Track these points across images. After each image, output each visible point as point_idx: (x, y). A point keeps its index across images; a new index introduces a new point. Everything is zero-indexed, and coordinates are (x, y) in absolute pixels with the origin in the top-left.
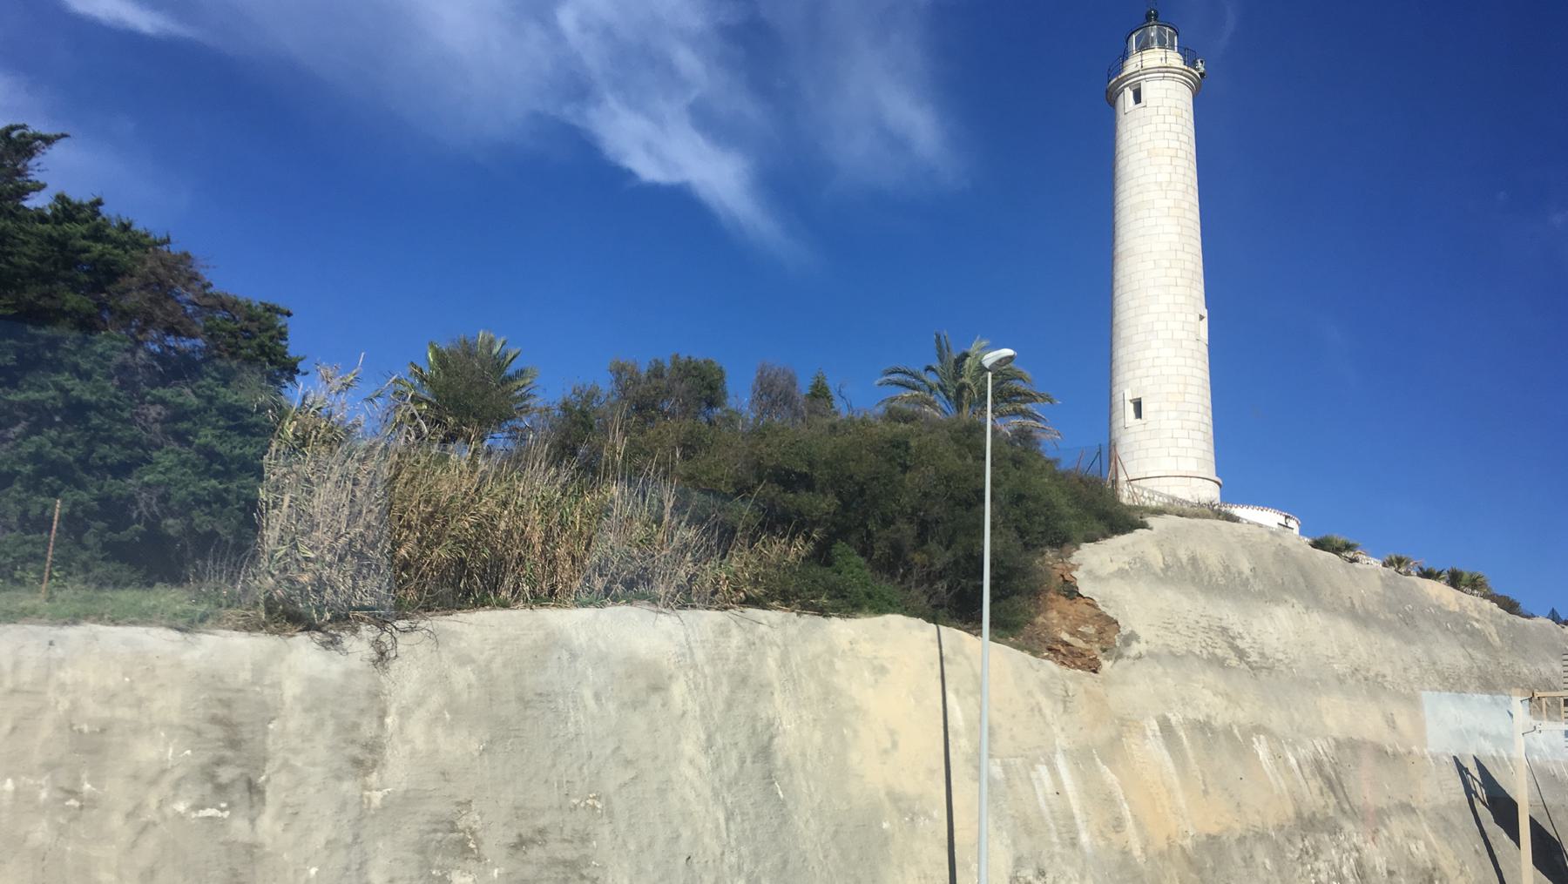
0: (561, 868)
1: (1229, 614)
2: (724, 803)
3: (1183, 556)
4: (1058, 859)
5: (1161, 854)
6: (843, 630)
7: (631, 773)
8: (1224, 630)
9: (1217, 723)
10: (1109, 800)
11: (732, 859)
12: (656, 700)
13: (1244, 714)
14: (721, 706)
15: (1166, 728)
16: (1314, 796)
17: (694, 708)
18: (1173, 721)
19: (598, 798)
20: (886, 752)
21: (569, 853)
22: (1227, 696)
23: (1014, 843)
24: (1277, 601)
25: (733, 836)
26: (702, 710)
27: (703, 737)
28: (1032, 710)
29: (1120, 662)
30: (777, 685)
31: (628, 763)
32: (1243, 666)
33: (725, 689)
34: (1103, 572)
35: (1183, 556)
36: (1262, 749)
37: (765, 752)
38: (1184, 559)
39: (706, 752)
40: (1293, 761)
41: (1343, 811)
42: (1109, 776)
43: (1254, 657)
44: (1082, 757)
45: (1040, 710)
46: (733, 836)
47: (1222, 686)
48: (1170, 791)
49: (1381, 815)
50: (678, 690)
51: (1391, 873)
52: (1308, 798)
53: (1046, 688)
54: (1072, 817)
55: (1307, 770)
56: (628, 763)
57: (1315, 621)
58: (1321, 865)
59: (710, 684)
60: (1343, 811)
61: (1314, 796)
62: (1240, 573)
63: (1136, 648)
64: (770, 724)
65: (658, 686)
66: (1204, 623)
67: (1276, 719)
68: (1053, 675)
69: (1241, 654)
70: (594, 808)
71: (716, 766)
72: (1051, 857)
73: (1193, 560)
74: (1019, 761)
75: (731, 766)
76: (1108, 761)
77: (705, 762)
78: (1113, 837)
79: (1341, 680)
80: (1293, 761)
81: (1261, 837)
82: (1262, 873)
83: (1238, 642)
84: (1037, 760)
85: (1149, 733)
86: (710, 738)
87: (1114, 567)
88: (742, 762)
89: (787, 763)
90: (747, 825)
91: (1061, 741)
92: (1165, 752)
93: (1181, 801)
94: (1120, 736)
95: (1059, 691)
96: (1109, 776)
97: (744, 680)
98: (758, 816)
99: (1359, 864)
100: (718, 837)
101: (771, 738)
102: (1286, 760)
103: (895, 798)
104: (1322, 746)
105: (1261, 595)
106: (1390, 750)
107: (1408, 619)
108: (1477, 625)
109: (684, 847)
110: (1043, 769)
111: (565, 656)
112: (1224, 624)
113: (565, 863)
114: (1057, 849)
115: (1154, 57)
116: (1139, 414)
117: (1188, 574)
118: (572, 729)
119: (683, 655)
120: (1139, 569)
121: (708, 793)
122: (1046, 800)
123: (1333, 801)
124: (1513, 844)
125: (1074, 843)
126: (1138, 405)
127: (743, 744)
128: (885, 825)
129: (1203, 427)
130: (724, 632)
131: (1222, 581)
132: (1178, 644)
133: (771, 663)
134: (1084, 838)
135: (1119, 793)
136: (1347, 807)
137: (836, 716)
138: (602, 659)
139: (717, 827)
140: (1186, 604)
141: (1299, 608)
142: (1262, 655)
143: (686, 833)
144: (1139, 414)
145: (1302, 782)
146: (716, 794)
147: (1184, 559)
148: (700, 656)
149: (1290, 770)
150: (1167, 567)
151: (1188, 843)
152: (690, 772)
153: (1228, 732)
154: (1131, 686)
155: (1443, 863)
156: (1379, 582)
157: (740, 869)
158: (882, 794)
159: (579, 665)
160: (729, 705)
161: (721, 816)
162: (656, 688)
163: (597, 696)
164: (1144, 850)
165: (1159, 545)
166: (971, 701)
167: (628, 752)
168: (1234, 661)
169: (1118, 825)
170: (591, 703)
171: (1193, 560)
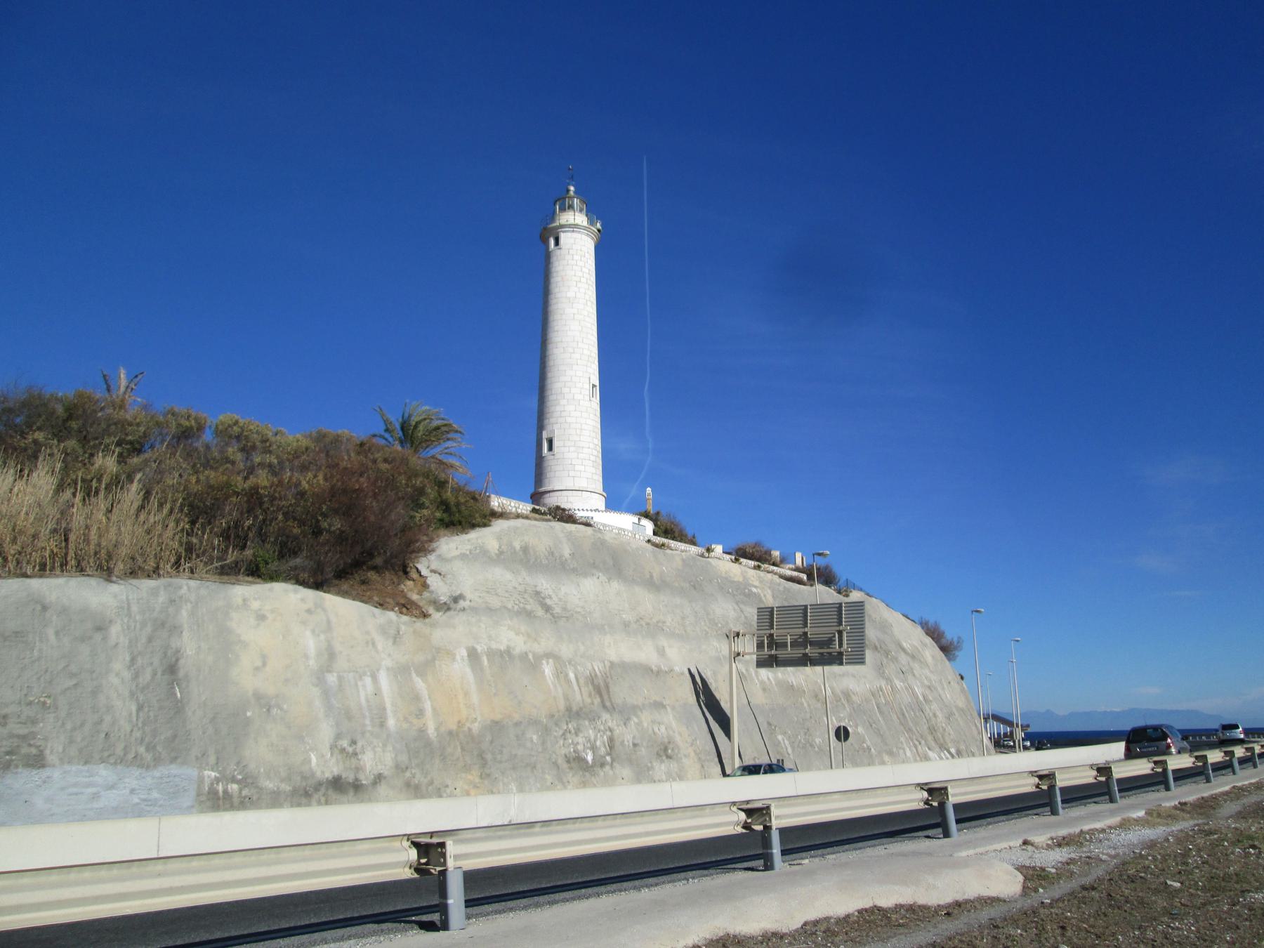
0: (15, 740)
1: (544, 584)
2: (137, 699)
3: (517, 545)
4: (368, 735)
5: (450, 733)
6: (247, 593)
7: (74, 682)
8: (538, 593)
9: (517, 652)
10: (417, 698)
11: (138, 734)
12: (98, 637)
13: (540, 648)
14: (144, 640)
15: (473, 655)
16: (581, 695)
17: (124, 641)
18: (479, 649)
19: (49, 697)
20: (257, 669)
21: (23, 731)
22: (529, 635)
23: (337, 725)
24: (585, 575)
25: (141, 720)
26: (130, 642)
27: (128, 658)
28: (367, 643)
29: (448, 613)
30: (185, 626)
31: (72, 675)
32: (549, 616)
33: (149, 629)
34: (449, 556)
35: (517, 545)
36: (548, 669)
37: (172, 669)
38: (518, 547)
39: (129, 668)
40: (572, 676)
41: (604, 706)
42: (419, 683)
43: (557, 610)
44: (401, 672)
45: (373, 644)
46: (141, 720)
47: (523, 628)
48: (466, 694)
49: (635, 709)
50: (115, 630)
51: (635, 745)
52: (578, 697)
53: (383, 630)
54: (384, 709)
55: (582, 681)
56: (72, 675)
57: (615, 585)
58: (580, 739)
59: (138, 626)
60: (604, 706)
61: (581, 695)
62: (561, 557)
63: (462, 604)
64: (178, 651)
65: (101, 627)
66: (521, 588)
67: (566, 650)
68: (390, 622)
69: (548, 609)
70: (44, 703)
71: (136, 676)
72: (363, 733)
73: (525, 549)
74: (351, 675)
75: (147, 676)
76: (421, 674)
77: (127, 675)
78: (415, 721)
79: (626, 625)
80: (572, 676)
81: (534, 722)
82: (529, 744)
83: (548, 602)
84: (365, 674)
85: (458, 657)
86: (133, 660)
87: (456, 553)
88: (155, 674)
89: (186, 676)
90: (151, 714)
91: (387, 663)
92: (468, 670)
93: (475, 699)
94: (434, 659)
95: (393, 632)
96: (419, 683)
97: (163, 624)
98: (161, 708)
99: (611, 740)
100: (130, 721)
101: (177, 660)
102: (567, 675)
103: (258, 696)
104: (598, 667)
105: (574, 570)
106: (654, 668)
107: (696, 586)
108: (754, 590)
109: (105, 727)
110: (368, 680)
111: (39, 608)
112: (538, 589)
113: (18, 736)
114: (369, 728)
115: (567, 218)
116: (550, 449)
117: (525, 559)
118: (36, 653)
119: (122, 608)
120: (481, 556)
121: (127, 693)
122: (368, 701)
123: (597, 700)
124: (570, 527)
125: (382, 725)
126: (550, 442)
127: (156, 661)
128: (249, 714)
129: (593, 458)
130: (154, 592)
131: (545, 562)
132: (495, 602)
133: (184, 613)
134: (391, 722)
135: (425, 694)
136: (608, 704)
137: (227, 645)
138: (64, 611)
139: (130, 715)
140: (508, 576)
141: (603, 578)
142: (565, 609)
143: (108, 719)
144: (550, 449)
145: (576, 688)
146: (132, 694)
147: (518, 547)
148: (134, 608)
149: (568, 681)
150: (501, 553)
151: (476, 727)
152: (115, 680)
153: (524, 657)
154: (450, 632)
155: (678, 739)
156: (680, 563)
157: (142, 740)
158: (250, 693)
159: (48, 615)
160: (150, 640)
161: (134, 708)
162: (99, 629)
163: (57, 633)
164: (437, 729)
165: (499, 538)
166: (322, 637)
167: (73, 668)
168: (540, 612)
169: (420, 713)
170: (52, 637)
171: (525, 549)
